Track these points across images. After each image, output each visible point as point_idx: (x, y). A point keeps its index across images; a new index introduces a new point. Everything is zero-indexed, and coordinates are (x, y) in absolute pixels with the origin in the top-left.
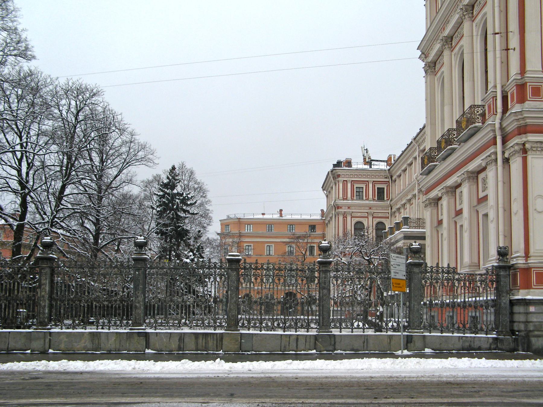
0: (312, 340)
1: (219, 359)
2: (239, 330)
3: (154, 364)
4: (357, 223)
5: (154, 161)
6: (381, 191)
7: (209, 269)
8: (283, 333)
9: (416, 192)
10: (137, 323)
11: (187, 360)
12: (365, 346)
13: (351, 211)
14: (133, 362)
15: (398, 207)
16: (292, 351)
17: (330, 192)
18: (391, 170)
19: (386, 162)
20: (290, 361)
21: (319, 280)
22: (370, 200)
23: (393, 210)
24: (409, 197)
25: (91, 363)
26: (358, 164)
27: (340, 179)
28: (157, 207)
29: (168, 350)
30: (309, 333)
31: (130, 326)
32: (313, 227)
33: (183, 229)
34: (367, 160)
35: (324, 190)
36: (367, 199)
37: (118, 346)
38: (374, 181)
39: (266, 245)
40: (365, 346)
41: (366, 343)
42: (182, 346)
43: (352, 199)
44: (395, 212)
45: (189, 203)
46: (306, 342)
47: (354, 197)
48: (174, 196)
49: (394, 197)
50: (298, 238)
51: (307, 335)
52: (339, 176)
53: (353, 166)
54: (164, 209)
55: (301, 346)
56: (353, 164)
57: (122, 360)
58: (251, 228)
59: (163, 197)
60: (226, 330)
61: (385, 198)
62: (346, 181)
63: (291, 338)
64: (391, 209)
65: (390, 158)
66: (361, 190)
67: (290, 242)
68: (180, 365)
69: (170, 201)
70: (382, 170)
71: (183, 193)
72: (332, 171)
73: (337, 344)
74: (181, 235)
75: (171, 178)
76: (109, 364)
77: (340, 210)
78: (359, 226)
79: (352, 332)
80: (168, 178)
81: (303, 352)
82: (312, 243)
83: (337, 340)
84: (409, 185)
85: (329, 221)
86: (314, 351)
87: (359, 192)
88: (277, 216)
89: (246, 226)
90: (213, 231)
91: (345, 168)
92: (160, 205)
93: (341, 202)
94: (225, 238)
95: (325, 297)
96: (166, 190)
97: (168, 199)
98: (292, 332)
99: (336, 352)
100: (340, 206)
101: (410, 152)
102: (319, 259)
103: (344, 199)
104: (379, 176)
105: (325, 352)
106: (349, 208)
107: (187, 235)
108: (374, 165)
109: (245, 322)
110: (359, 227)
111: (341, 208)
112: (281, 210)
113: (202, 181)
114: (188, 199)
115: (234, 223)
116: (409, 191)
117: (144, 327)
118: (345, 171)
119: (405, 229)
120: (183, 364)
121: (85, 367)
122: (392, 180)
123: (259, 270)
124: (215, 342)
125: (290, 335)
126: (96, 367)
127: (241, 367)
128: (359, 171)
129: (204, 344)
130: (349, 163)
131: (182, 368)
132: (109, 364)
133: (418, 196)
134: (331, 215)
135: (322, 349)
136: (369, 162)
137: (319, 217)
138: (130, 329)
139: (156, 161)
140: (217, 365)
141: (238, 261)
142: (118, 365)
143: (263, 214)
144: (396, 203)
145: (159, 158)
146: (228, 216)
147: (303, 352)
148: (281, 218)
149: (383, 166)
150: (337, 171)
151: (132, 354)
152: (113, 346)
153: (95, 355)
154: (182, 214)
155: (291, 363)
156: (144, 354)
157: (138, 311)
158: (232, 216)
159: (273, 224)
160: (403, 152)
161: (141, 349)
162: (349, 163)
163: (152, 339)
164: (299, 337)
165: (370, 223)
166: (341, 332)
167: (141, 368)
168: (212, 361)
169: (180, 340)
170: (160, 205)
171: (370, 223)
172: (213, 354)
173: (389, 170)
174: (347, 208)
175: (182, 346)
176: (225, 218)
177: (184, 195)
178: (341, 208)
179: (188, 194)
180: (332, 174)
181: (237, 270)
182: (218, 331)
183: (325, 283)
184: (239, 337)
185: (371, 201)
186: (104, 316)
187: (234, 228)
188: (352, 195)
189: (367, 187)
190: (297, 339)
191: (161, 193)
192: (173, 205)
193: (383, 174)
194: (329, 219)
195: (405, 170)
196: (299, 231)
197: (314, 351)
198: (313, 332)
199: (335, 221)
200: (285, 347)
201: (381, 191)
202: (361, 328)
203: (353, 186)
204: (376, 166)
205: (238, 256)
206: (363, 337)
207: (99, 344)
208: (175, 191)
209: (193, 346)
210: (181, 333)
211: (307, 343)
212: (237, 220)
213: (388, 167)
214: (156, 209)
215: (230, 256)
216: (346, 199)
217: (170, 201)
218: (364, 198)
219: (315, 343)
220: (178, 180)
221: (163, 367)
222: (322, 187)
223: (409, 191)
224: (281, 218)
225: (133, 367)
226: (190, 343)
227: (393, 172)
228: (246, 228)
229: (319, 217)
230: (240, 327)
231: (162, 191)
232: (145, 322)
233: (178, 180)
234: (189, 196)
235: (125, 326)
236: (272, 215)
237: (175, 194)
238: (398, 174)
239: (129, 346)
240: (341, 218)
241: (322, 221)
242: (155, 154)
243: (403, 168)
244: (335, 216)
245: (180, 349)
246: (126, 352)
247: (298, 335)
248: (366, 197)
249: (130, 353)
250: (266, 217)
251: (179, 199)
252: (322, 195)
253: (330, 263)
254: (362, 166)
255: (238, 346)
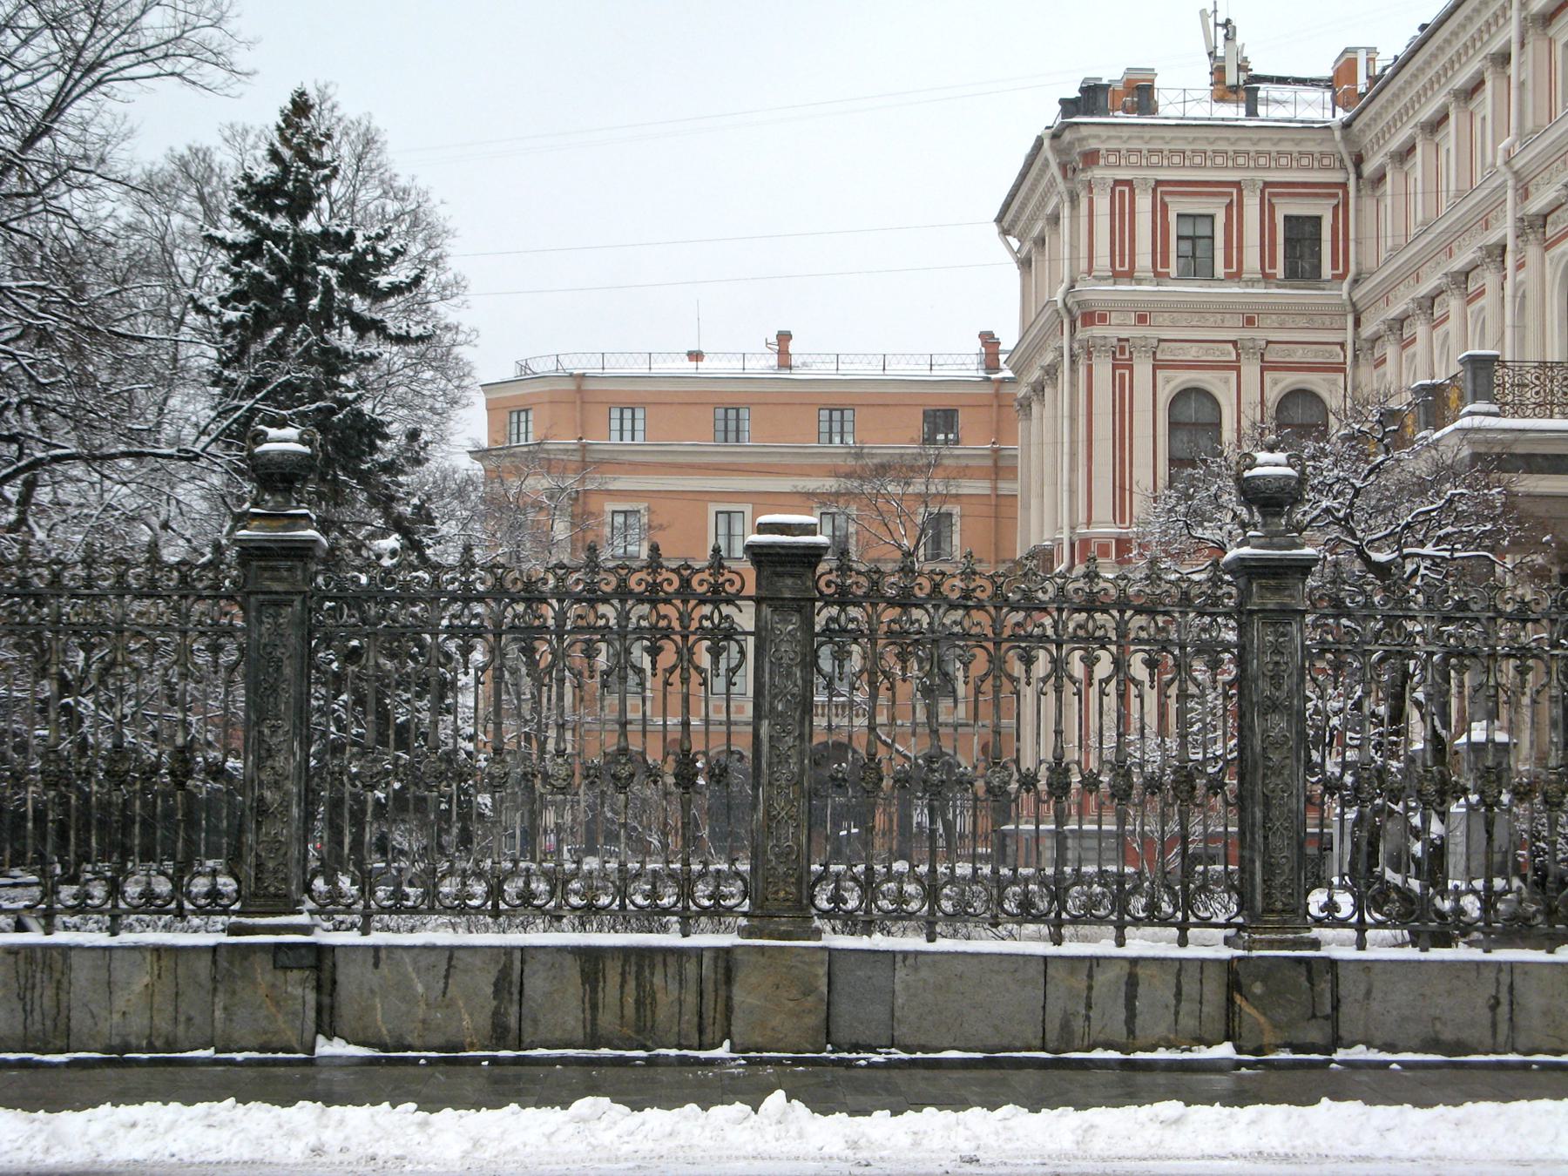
0: (1214, 992)
1: (779, 1095)
2: (817, 933)
3: (424, 1125)
4: (1185, 395)
5: (235, 58)
6: (1302, 234)
7: (654, 602)
8: (1049, 949)
9: (1505, 229)
10: (267, 897)
11: (605, 1101)
12: (1503, 1027)
13: (1152, 333)
14: (305, 1112)
15: (1395, 311)
16: (1107, 1046)
17: (1040, 242)
18: (1358, 125)
19: (1329, 84)
20: (1172, 1108)
21: (1241, 661)
22: (1248, 283)
23: (1367, 331)
24: (1459, 263)
25: (69, 1120)
26: (1185, 93)
27: (1097, 173)
28: (224, 302)
29: (439, 1039)
30: (1191, 952)
31: (225, 911)
32: (941, 419)
33: (360, 414)
34: (1231, 78)
35: (1005, 232)
36: (1236, 276)
37: (163, 1024)
38: (1267, 184)
39: (713, 508)
40: (1503, 1027)
41: (1504, 1009)
42: (513, 1022)
43: (1160, 276)
44: (1375, 339)
45: (383, 282)
46: (1178, 994)
47: (1165, 263)
48: (306, 247)
49: (1370, 263)
50: (882, 470)
51: (1180, 960)
52: (1091, 158)
53: (1163, 110)
54: (258, 312)
55: (1153, 1020)
56: (1161, 98)
57: (243, 1099)
58: (639, 425)
59: (252, 250)
60: (746, 932)
61: (1327, 271)
62: (1129, 183)
63: (1101, 978)
64: (1357, 323)
65: (1347, 65)
66: (1203, 230)
67: (838, 494)
68: (570, 1129)
69: (286, 276)
70: (1308, 127)
71: (351, 236)
72: (1056, 136)
73: (1343, 1009)
74: (349, 441)
75: (287, 153)
76: (172, 1126)
77: (1097, 331)
78: (1191, 411)
79: (1361, 945)
80: (275, 156)
81: (1162, 1054)
82: (946, 498)
83: (1350, 988)
84: (1461, 195)
85: (1039, 389)
86: (1225, 1051)
87: (1193, 239)
88: (763, 364)
89: (616, 414)
90: (461, 440)
91: (1120, 117)
92: (239, 297)
93: (1100, 291)
94: (518, 471)
95: (1275, 757)
96: (265, 218)
97: (276, 265)
98: (1103, 945)
99: (1341, 1054)
100: (1098, 309)
101: (1472, 30)
102: (1246, 551)
103: (1116, 276)
104: (1296, 159)
105: (1285, 1055)
106: (1142, 319)
107: (374, 448)
108: (1267, 102)
109: (540, 886)
110: (1193, 419)
111: (1103, 318)
112: (784, 337)
113: (422, 183)
114: (380, 264)
115: (555, 400)
116: (1462, 230)
117: (303, 919)
118: (1125, 133)
119: (1477, 418)
120: (584, 1120)
121: (39, 1142)
122: (1359, 176)
123: (857, 604)
124: (691, 999)
125: (1095, 961)
126: (102, 1145)
127: (905, 1141)
128: (1190, 134)
129: (630, 1011)
130: (1141, 93)
131: (579, 1147)
132: (172, 1126)
133: (1518, 250)
134: (1049, 358)
135: (1268, 1038)
136: (1240, 85)
137: (972, 369)
138: (233, 930)
139: (242, 59)
140: (771, 1131)
141: (812, 555)
142: (226, 1134)
143: (696, 356)
144: (1385, 294)
145: (249, 45)
146: (524, 367)
147: (1162, 1054)
148: (785, 374)
149: (1315, 107)
150: (1084, 131)
151: (248, 1063)
152: (138, 1024)
153: (40, 1075)
154: (345, 339)
155: (1178, 1121)
156: (310, 1062)
157: (271, 829)
158: (543, 367)
159: (748, 406)
160: (1429, 32)
161: (291, 1037)
162: (1141, 93)
163: (350, 978)
164: (1140, 971)
165: (1242, 400)
166: (1121, 942)
167: (356, 1151)
168: (739, 1109)
169: (502, 985)
170: (239, 297)
171: (1242, 400)
172: (683, 1061)
173: (1347, 125)
174: (1132, 318)
175: (513, 1022)
176: (510, 373)
177: (360, 244)
178: (1103, 318)
179: (379, 238)
180: (1058, 151)
181: (803, 606)
182: (705, 939)
183: (1276, 679)
184: (822, 971)
185: (1252, 282)
186: (147, 855)
187: (568, 415)
188: (1160, 254)
189: (1235, 210)
190: (1132, 982)
191: (242, 235)
192: (304, 292)
193: (1317, 149)
194: (1035, 374)
195: (1436, 125)
196: (899, 439)
197: (1225, 1051)
198: (1210, 946)
199: (1073, 385)
200: (1066, 1026)
201: (1302, 234)
202: (1343, 923)
203: (1165, 206)
204: (1279, 107)
205: (808, 529)
206: (1490, 974)
207: (61, 1014)
208: (310, 225)
209: (571, 1018)
210: (508, 951)
211: (1185, 1007)
212: (570, 386)
213: (1341, 115)
214: (219, 315)
215: (764, 528)
216: (1130, 275)
217: (286, 276)
218: (1220, 270)
219: (1230, 1001)
220: (324, 166)
221: (476, 1144)
222: (999, 220)
223: (1462, 230)
224: (785, 374)
225: (312, 1140)
226: (560, 1004)
227: (1370, 135)
228: (615, 424)
229: (972, 369)
230: (824, 914)
231: (249, 223)
232: (308, 889)
233: (324, 166)
234: (381, 248)
235: (200, 911)
236: (739, 355)
237: (309, 236)
238: (1395, 143)
239: (229, 1019)
240: (1103, 370)
241: (988, 390)
242: (230, 26)
243: (1427, 112)
244: (1073, 362)
245: (500, 1036)
246: (209, 1053)
247: (1134, 961)
248: (1228, 264)
249: (232, 1062)
250: (708, 367)
251: (332, 264)
252: (997, 263)
253: (1304, 567)
254: (1204, 108)
255: (814, 1020)
